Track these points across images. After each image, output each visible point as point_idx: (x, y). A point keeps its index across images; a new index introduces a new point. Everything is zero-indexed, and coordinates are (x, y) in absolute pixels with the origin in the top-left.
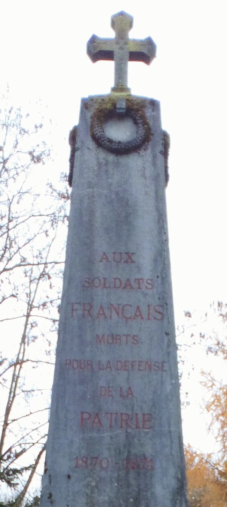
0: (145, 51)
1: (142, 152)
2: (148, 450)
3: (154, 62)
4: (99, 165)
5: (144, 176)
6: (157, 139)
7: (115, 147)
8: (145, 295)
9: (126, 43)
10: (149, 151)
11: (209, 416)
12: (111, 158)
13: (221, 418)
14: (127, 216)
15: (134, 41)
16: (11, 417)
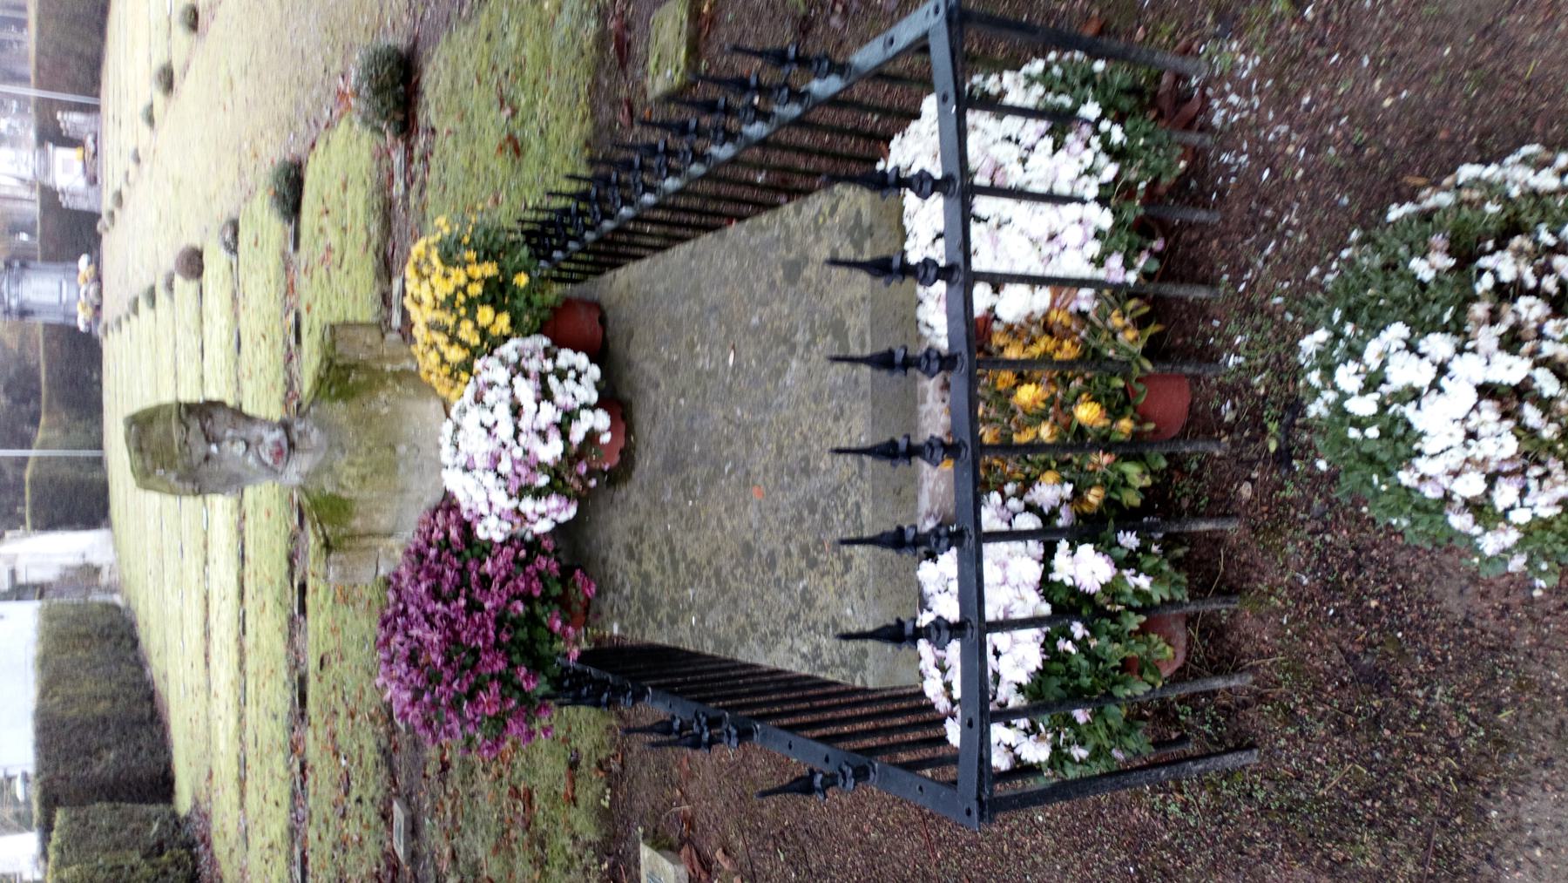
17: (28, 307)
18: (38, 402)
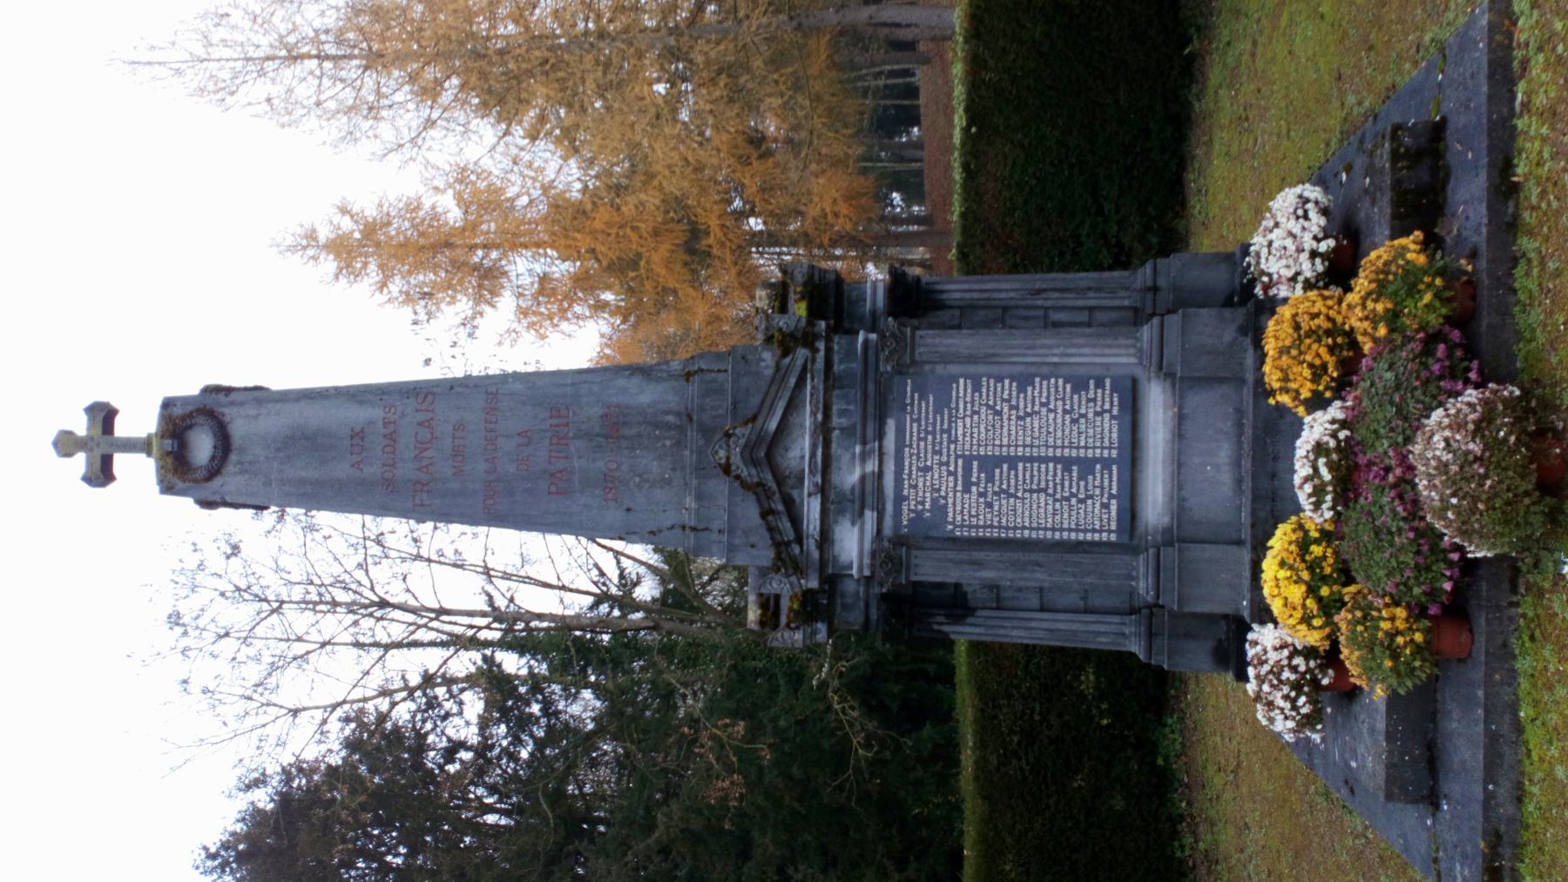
0: (101, 416)
1: (227, 419)
2: (596, 411)
3: (115, 404)
4: (242, 472)
5: (256, 417)
6: (210, 401)
9: (92, 439)
10: (226, 410)
12: (233, 457)
13: (555, 321)
14: (306, 438)
15: (89, 429)
16: (555, 582)
17: (930, 569)
18: (944, 714)
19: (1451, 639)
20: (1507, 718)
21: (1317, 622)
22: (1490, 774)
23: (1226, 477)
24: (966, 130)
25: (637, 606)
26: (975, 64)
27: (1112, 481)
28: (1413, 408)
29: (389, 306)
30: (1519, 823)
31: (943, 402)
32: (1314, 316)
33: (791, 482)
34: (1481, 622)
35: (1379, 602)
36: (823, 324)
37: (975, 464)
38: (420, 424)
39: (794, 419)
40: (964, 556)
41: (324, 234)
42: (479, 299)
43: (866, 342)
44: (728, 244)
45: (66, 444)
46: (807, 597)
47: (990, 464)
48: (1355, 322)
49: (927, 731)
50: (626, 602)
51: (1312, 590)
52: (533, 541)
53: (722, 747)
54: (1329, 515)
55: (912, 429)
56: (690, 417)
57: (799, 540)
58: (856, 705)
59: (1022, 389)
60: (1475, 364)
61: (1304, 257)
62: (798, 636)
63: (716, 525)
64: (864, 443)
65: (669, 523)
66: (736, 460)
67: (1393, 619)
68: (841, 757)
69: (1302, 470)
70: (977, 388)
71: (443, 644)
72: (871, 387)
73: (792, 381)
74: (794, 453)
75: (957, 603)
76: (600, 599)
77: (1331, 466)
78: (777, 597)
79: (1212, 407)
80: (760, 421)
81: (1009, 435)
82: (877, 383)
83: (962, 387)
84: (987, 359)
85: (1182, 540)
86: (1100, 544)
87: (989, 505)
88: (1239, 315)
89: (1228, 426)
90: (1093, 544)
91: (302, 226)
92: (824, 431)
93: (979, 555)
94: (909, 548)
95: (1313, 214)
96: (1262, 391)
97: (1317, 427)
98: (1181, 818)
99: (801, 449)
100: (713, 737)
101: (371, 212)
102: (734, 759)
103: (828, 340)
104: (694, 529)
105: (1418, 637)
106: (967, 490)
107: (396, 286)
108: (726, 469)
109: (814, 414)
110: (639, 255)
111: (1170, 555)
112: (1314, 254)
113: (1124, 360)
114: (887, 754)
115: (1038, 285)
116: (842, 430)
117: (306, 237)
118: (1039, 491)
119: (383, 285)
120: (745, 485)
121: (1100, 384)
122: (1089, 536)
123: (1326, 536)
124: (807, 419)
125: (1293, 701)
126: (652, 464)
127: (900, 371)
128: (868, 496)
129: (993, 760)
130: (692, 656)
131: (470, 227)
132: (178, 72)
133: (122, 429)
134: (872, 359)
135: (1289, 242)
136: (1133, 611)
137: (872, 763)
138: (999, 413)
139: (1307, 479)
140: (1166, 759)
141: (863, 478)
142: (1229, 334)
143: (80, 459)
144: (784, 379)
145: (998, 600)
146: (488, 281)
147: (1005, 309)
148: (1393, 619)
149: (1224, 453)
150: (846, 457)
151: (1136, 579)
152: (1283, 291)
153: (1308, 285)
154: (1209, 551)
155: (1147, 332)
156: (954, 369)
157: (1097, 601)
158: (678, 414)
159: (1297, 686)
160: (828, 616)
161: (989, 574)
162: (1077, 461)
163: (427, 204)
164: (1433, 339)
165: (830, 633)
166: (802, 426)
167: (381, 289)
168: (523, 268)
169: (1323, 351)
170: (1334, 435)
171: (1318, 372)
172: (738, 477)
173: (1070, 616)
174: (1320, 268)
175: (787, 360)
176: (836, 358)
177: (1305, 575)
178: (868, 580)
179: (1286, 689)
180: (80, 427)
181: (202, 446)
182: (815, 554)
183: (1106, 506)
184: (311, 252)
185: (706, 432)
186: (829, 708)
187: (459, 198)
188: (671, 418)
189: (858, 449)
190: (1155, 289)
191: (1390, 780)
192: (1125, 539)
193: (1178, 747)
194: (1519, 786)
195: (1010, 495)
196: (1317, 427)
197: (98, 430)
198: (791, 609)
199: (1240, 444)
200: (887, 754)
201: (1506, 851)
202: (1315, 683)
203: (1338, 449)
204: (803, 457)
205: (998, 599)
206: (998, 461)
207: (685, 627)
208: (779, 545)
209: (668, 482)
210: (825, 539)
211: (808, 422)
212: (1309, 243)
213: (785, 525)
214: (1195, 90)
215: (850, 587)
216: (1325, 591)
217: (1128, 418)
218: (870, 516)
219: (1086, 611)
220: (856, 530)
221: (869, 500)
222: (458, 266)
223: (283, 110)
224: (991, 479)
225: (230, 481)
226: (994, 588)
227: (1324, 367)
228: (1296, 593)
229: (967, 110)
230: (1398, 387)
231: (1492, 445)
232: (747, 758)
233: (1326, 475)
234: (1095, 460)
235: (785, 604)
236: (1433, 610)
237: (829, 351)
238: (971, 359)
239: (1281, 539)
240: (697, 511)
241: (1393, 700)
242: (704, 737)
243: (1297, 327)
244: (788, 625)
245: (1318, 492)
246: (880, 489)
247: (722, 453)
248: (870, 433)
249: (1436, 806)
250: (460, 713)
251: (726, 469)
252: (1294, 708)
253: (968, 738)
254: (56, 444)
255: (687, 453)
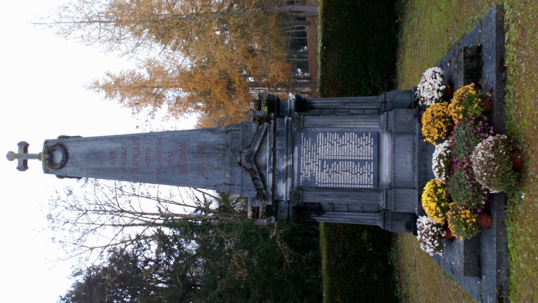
0: (23, 146)
1: (67, 147)
2: (195, 144)
3: (28, 142)
4: (73, 166)
5: (77, 147)
6: (61, 141)
7: (65, 159)
8: (129, 146)
9: (20, 154)
10: (67, 144)
11: (181, 118)
12: (70, 160)
13: (182, 113)
15: (19, 151)
16: (182, 203)
17: (310, 198)
18: (316, 248)
19: (485, 221)
20: (504, 247)
21: (440, 215)
22: (498, 267)
23: (410, 166)
24: (322, 48)
25: (210, 211)
26: (325, 26)
27: (371, 167)
28: (471, 142)
29: (124, 108)
30: (508, 283)
31: (314, 141)
32: (439, 111)
33: (262, 168)
34: (495, 215)
35: (461, 208)
36: (273, 114)
37: (325, 162)
38: (134, 149)
39: (263, 147)
40: (321, 193)
41: (101, 83)
42: (155, 105)
43: (288, 120)
44: (241, 86)
45: (11, 156)
46: (268, 207)
47: (330, 162)
48: (452, 113)
49: (310, 253)
50: (207, 210)
51: (438, 204)
52: (174, 189)
53: (240, 259)
54: (444, 179)
55: (303, 150)
56: (228, 146)
57: (265, 188)
58: (286, 244)
59: (340, 136)
60: (492, 128)
61: (435, 91)
62: (265, 221)
63: (237, 183)
64: (287, 155)
65: (220, 183)
66: (244, 161)
67: (465, 214)
68: (281, 263)
69: (435, 164)
70: (325, 136)
71: (143, 225)
72: (289, 136)
73: (263, 134)
74: (263, 159)
75: (319, 209)
76: (198, 209)
77: (444, 162)
78: (258, 208)
79: (405, 143)
80: (251, 148)
81: (337, 152)
82: (292, 134)
83: (320, 136)
84: (329, 126)
85: (395, 188)
86: (367, 189)
87: (330, 176)
88: (414, 111)
89: (410, 149)
90: (365, 189)
91: (94, 80)
92: (273, 151)
93: (326, 193)
94: (303, 191)
95: (438, 77)
96: (421, 137)
97: (440, 149)
98: (397, 282)
99: (266, 157)
100: (237, 256)
101: (118, 75)
102: (244, 264)
103: (275, 120)
104: (229, 185)
105: (474, 220)
106: (322, 171)
107: (126, 101)
108: (240, 164)
109: (270, 145)
110: (211, 90)
111: (391, 192)
112: (438, 91)
113: (375, 126)
114: (297, 261)
115: (346, 101)
116: (279, 150)
117: (95, 84)
118: (347, 171)
119: (122, 101)
120: (246, 169)
121: (367, 135)
122: (364, 186)
123: (443, 186)
124: (268, 147)
125: (433, 242)
126: (215, 163)
127: (300, 130)
128: (289, 173)
129: (333, 263)
130: (230, 228)
131: (152, 80)
132: (50, 27)
133: (30, 151)
134: (290, 126)
135: (430, 87)
136: (379, 212)
137: (292, 265)
138: (333, 145)
139: (436, 167)
140: (391, 262)
141: (287, 167)
142: (410, 117)
143: (16, 162)
144: (259, 133)
145: (333, 208)
146: (158, 99)
147: (335, 109)
148: (465, 214)
149: (409, 158)
150: (281, 160)
151: (379, 201)
152: (428, 103)
153: (437, 101)
154: (404, 191)
155: (383, 117)
156: (317, 129)
157: (366, 208)
158: (223, 145)
159: (434, 237)
160: (275, 214)
161: (330, 199)
162: (359, 161)
163: (137, 72)
164: (478, 119)
165: (276, 220)
166: (266, 149)
167: (121, 102)
168: (171, 94)
169: (441, 123)
170: (445, 152)
171: (440, 130)
172: (244, 167)
173: (357, 214)
174: (440, 95)
175: (261, 127)
176: (277, 126)
177: (436, 199)
178: (289, 202)
179: (430, 238)
180: (16, 150)
181: (59, 157)
182: (271, 193)
183: (369, 176)
184: (97, 89)
185: (233, 151)
186: (277, 246)
187: (148, 71)
188: (221, 147)
189: (285, 157)
190: (385, 102)
191: (465, 268)
192: (376, 188)
193: (395, 258)
194: (508, 270)
195: (337, 173)
196: (440, 149)
197: (22, 151)
198: (263, 212)
199: (414, 155)
200: (297, 261)
201: (504, 292)
202: (440, 235)
203: (447, 157)
204: (266, 160)
205: (333, 208)
206: (333, 161)
207: (227, 218)
208: (258, 190)
209: (221, 168)
210: (274, 188)
211: (268, 148)
212: (437, 87)
213: (260, 183)
214: (399, 34)
215: (283, 204)
216: (443, 205)
217: (376, 146)
218: (289, 180)
219: (363, 212)
220: (285, 184)
221: (289, 174)
222: (148, 94)
223: (87, 40)
224: (330, 167)
225: (68, 169)
226: (332, 204)
227: (442, 129)
228: (433, 205)
229: (322, 41)
230: (466, 136)
231: (498, 155)
232: (249, 264)
233: (443, 165)
234: (365, 160)
235: (261, 210)
236: (479, 211)
237: (275, 123)
238: (323, 126)
239: (428, 187)
240: (230, 178)
241: (466, 241)
242: (234, 256)
243: (433, 115)
244: (262, 217)
245: (440, 171)
246: (293, 171)
247: (239, 159)
248: (289, 151)
249: (481, 277)
250: (150, 249)
251: (240, 164)
252: (433, 244)
253: (324, 256)
254: (7, 156)
255: (227, 158)
